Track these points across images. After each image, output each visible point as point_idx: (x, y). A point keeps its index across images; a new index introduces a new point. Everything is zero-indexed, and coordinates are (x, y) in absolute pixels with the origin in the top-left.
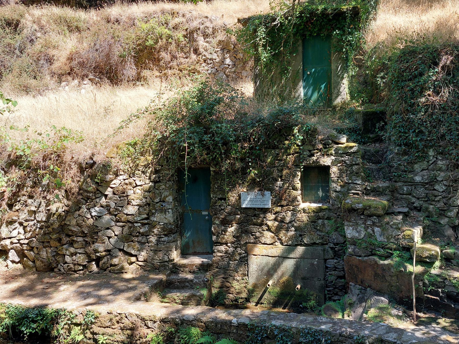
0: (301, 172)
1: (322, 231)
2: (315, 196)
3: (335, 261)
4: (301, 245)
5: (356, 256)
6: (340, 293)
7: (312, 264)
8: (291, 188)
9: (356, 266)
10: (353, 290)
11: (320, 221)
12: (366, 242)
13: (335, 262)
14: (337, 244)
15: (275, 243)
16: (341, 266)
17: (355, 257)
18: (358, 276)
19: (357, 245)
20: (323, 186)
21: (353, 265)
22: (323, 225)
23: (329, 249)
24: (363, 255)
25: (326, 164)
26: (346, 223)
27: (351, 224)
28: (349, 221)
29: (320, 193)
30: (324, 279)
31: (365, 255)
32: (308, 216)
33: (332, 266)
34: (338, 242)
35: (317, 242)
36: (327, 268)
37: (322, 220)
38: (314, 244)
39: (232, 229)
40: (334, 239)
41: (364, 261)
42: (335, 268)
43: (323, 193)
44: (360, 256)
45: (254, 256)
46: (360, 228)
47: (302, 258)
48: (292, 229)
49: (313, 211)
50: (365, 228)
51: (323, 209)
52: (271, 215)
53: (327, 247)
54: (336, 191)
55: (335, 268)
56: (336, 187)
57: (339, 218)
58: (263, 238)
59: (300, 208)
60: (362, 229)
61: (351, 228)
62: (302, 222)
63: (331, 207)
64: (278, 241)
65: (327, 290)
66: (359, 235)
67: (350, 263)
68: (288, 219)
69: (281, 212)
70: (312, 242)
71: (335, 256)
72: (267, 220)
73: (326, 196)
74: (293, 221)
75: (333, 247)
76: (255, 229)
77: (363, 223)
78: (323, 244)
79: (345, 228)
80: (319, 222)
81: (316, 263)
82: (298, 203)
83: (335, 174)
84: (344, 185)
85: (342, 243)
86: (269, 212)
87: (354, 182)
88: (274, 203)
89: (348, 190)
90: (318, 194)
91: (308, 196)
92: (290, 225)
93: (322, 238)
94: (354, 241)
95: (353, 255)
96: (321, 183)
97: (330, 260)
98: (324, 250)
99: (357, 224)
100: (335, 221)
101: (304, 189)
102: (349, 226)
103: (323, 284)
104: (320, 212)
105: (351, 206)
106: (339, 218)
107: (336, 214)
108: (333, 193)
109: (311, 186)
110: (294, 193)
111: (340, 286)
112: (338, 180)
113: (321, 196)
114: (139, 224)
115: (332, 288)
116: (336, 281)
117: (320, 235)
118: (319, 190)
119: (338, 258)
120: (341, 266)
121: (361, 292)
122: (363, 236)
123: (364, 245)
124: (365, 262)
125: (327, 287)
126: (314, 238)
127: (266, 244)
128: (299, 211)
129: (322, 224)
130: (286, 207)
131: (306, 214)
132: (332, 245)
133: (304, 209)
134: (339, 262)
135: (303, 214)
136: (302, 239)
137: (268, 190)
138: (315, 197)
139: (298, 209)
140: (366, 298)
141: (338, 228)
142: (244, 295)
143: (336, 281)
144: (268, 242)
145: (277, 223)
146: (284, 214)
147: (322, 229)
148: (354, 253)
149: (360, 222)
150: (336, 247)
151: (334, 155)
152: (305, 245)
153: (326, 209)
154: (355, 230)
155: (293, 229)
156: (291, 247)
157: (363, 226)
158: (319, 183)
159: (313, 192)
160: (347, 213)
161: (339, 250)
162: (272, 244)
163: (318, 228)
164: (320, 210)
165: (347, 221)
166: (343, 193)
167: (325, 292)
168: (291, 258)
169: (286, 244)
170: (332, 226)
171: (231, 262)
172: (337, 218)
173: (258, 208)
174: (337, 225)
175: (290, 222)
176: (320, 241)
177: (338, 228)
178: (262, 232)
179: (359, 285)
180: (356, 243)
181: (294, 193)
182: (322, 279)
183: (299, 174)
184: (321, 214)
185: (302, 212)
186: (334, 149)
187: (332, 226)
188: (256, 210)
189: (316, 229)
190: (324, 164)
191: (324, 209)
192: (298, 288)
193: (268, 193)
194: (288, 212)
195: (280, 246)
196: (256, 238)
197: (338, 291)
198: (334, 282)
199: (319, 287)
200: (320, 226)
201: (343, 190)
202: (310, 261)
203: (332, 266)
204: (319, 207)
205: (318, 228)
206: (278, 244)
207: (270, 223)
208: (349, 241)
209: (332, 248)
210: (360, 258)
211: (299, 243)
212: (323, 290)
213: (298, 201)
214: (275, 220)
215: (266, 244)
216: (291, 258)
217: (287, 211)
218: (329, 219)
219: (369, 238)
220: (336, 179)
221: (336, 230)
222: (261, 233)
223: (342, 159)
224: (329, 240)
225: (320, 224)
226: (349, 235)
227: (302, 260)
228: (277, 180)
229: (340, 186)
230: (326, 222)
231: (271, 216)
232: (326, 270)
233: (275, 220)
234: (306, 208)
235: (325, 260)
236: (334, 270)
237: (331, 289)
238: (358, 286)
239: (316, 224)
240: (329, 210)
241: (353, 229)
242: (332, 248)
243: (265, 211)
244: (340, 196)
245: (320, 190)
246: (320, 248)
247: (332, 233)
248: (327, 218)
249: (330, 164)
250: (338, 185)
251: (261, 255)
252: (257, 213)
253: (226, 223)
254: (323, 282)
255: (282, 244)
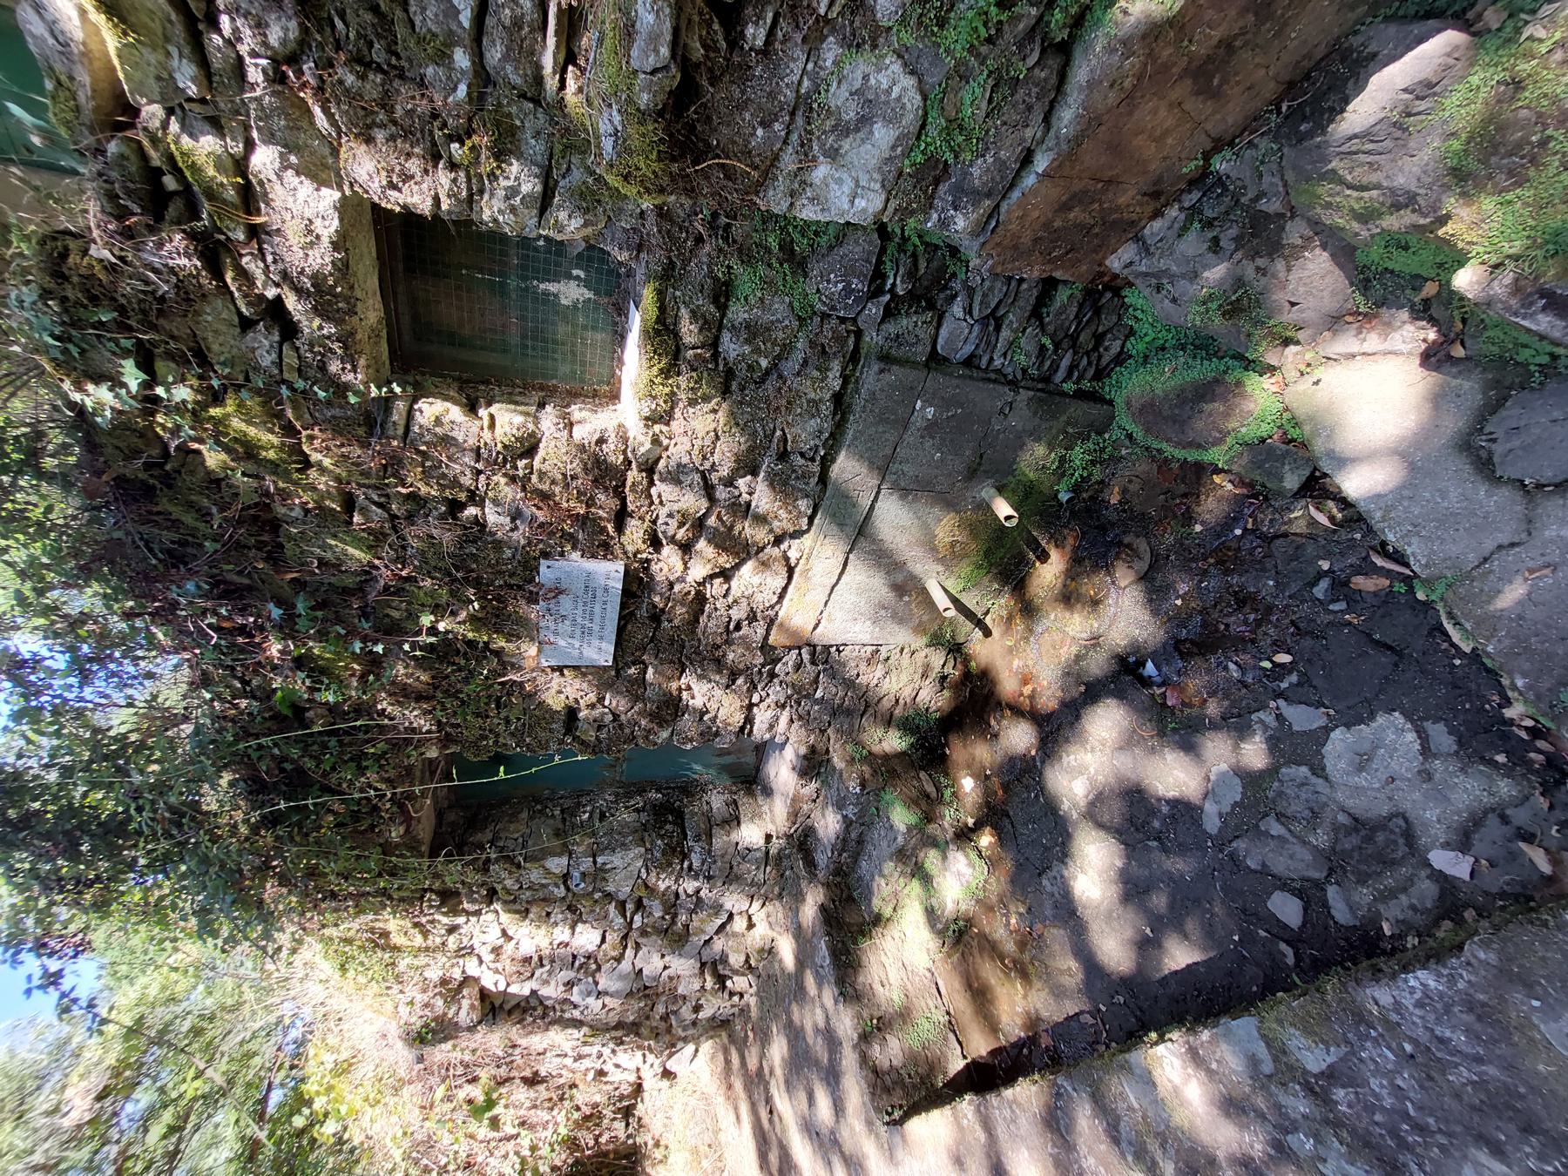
0: (419, 392)
1: (787, 348)
2: (585, 328)
3: (957, 309)
4: (826, 463)
5: (1012, 186)
6: (1107, 321)
7: (932, 427)
8: (521, 464)
9: (1065, 207)
10: (1163, 265)
11: (731, 347)
12: (962, 74)
13: (960, 315)
14: (878, 275)
15: (787, 559)
16: (998, 284)
17: (1016, 194)
18: (1118, 209)
19: (949, 157)
20: (524, 267)
21: (1047, 225)
22: (752, 332)
23: (891, 328)
24: (1029, 133)
25: (328, 228)
26: (775, 200)
27: (789, 162)
28: (765, 174)
29: (571, 292)
30: (1013, 384)
31: (1037, 117)
32: (692, 403)
33: (974, 334)
34: (869, 269)
35: (836, 385)
36: (969, 362)
37: (726, 337)
38: (839, 401)
39: (700, 692)
40: (848, 290)
41: (1077, 141)
42: (993, 321)
43: (569, 277)
44: (1027, 159)
45: (818, 630)
46: (844, 93)
47: (884, 468)
48: (744, 489)
49: (666, 373)
50: (853, 44)
51: (661, 319)
52: (661, 564)
53: (872, 338)
54: (544, 202)
55: (993, 321)
56: (512, 192)
57: (728, 226)
58: (759, 597)
59: (641, 438)
60: (860, 67)
61: (821, 172)
62: (717, 438)
63: (654, 259)
64: (784, 546)
65: (1064, 381)
66: (888, 121)
67: (1026, 240)
68: (692, 502)
69: (654, 522)
70: (826, 408)
71: (931, 306)
72: (681, 580)
73: (590, 259)
74: (704, 478)
75: (887, 307)
76: (710, 624)
77: (813, 45)
78: (854, 357)
79: (808, 213)
80: (733, 354)
81: (930, 411)
82: (612, 439)
83: (407, 178)
84: (498, 124)
85: (883, 251)
86: (646, 570)
87: (466, 18)
88: (603, 548)
89: (536, 102)
90: (575, 306)
91: (583, 364)
92: (722, 493)
93: (824, 352)
94: (919, 174)
95: (998, 206)
96: (502, 274)
97: (944, 332)
98: (886, 358)
99: (804, 106)
100: (746, 257)
101: (544, 376)
102: (800, 185)
103: (1031, 393)
104: (676, 336)
105: (643, 116)
106: (728, 226)
107: (699, 240)
108: (560, 228)
109: (524, 337)
110: (554, 455)
111: (1077, 317)
112: (453, 166)
113: (589, 295)
114: (638, 918)
115: (1069, 355)
116: (1050, 329)
117: (805, 363)
118: (546, 293)
119: (945, 287)
120: (998, 284)
121: (1209, 224)
122: (909, 82)
123: (972, 99)
124: (1091, 123)
125: (1047, 379)
126: (812, 395)
127: (785, 589)
128: (656, 441)
129: (747, 341)
130: (630, 498)
131: (678, 413)
132: (874, 310)
133: (647, 419)
134: (971, 292)
135: (677, 425)
136: (802, 455)
137: (529, 567)
138: (594, 328)
139: (648, 446)
140: (1272, 206)
141: (787, 248)
142: (937, 659)
143: (1050, 329)
144: (779, 582)
145: (702, 544)
146: (663, 512)
147: (774, 344)
148: (989, 195)
149: (795, 66)
150: (894, 285)
151: (237, 148)
152: (833, 443)
153: (661, 294)
154: (846, 145)
155: (742, 483)
156: (826, 502)
157: (831, 51)
158: (503, 285)
159: (562, 330)
160: (705, 174)
161: (912, 274)
162: (791, 571)
163: (764, 363)
164: (663, 335)
165: (759, 187)
166: (558, 148)
167: (1064, 394)
168: (872, 507)
169: (806, 520)
170: (771, 283)
171: (819, 694)
172: (725, 239)
173: (623, 606)
174: (768, 250)
175: (709, 490)
176: (836, 367)
177: (787, 248)
178: (730, 599)
179: (1157, 214)
180: (932, 161)
181: (554, 455)
182: (1010, 396)
183: (542, 286)
184: (689, 332)
185: (665, 429)
186: (174, 126)
187: (771, 283)
188: (632, 614)
189: (767, 372)
190: (325, 241)
191: (662, 309)
192: (1008, 518)
193: (547, 572)
194: (654, 491)
195: (807, 540)
196: (752, 617)
197: (1094, 327)
198: (1047, 342)
199: (1035, 414)
200: (757, 351)
201: (535, 147)
202: (909, 438)
203: (974, 334)
204: (645, 333)
205: (764, 363)
206: (794, 549)
207: (698, 571)
208: (904, 212)
209: (889, 313)
210: (1041, 163)
211: (815, 468)
212: (1058, 399)
213: (601, 441)
214: (686, 548)
215: (785, 589)
216: (872, 507)
217: (650, 496)
218: (722, 293)
219: (942, 23)
220: (444, 177)
221: (799, 265)
222: (735, 602)
223: (254, 75)
224: (843, 320)
225: (747, 349)
226: (861, 203)
227: (894, 467)
228: (480, 524)
229: (500, 155)
230: (738, 313)
231: (668, 562)
232: (978, 368)
233: (686, 548)
234: (646, 408)
235: (935, 360)
236: (998, 329)
237: (1065, 363)
238: (1157, 224)
239: (742, 372)
240: (667, 276)
241: (833, 155)
242: (889, 313)
243: (637, 583)
244: (577, 175)
245: (552, 287)
246: (870, 377)
247: (811, 290)
248: (715, 301)
249: (331, 196)
250: (492, 176)
251: (821, 606)
252: (643, 612)
253: (671, 708)
254: (1024, 395)
255: (797, 534)
